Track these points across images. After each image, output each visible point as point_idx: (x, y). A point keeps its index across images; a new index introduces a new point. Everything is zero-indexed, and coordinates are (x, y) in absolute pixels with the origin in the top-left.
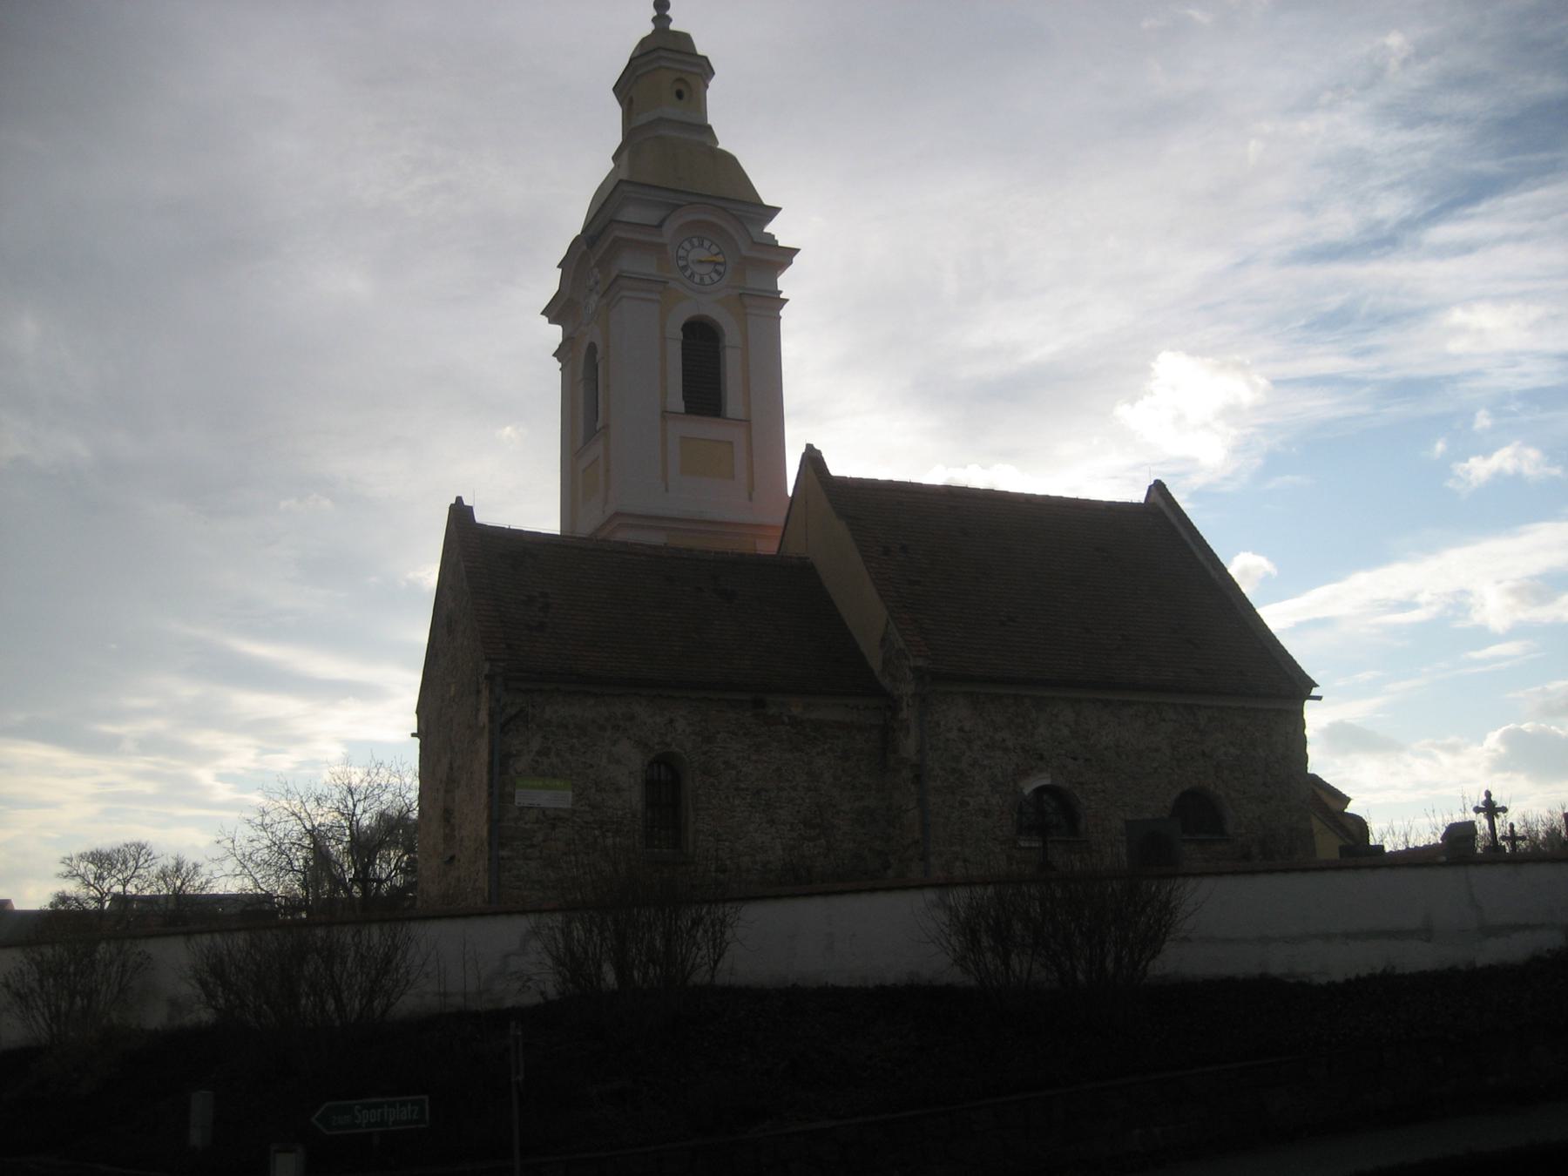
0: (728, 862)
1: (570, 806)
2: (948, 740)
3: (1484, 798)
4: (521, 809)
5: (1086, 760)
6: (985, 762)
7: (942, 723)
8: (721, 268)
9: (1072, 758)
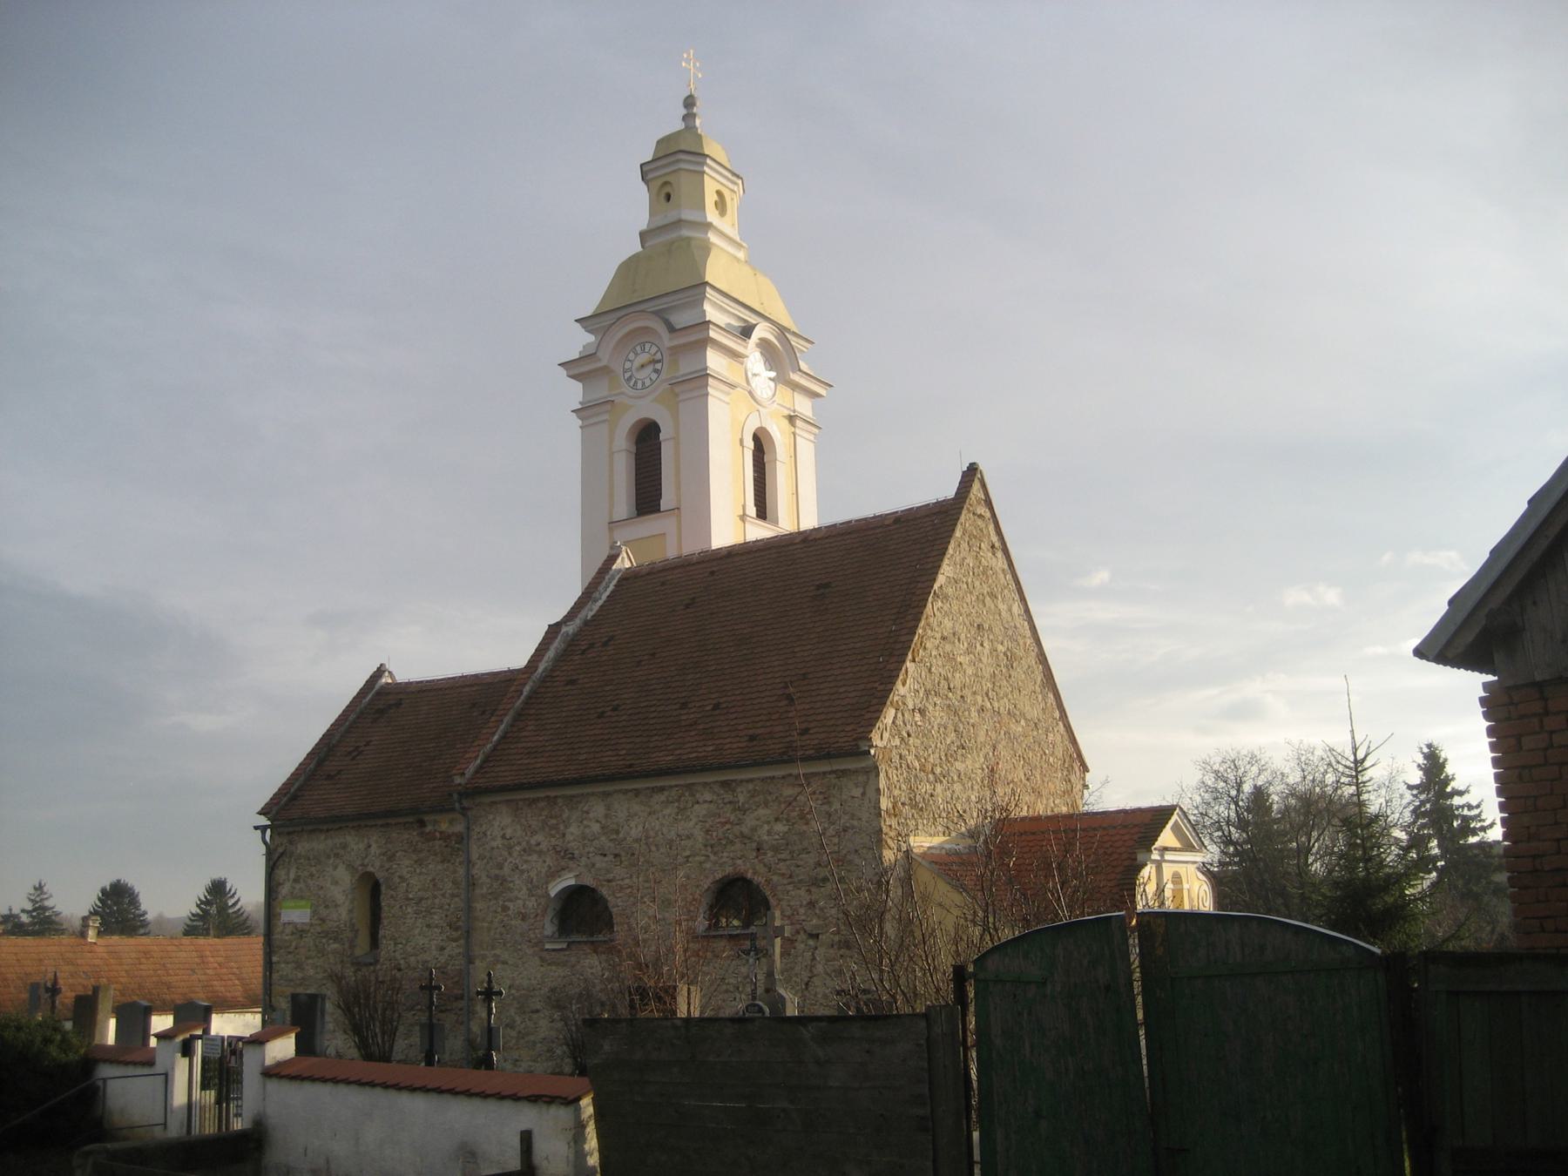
0: (402, 962)
1: (308, 921)
2: (493, 848)
3: (1416, 777)
4: (285, 924)
5: (616, 856)
6: (525, 867)
7: (489, 833)
8: (658, 366)
9: (601, 854)
